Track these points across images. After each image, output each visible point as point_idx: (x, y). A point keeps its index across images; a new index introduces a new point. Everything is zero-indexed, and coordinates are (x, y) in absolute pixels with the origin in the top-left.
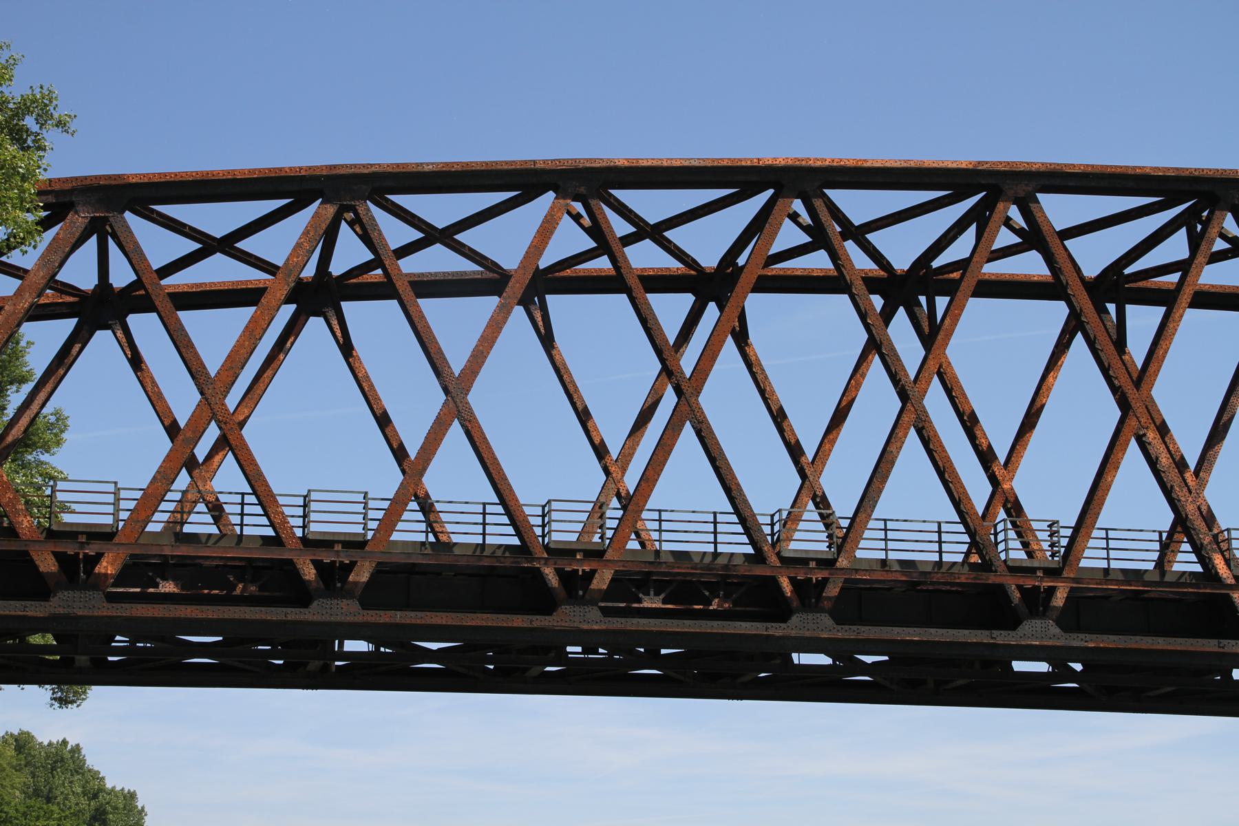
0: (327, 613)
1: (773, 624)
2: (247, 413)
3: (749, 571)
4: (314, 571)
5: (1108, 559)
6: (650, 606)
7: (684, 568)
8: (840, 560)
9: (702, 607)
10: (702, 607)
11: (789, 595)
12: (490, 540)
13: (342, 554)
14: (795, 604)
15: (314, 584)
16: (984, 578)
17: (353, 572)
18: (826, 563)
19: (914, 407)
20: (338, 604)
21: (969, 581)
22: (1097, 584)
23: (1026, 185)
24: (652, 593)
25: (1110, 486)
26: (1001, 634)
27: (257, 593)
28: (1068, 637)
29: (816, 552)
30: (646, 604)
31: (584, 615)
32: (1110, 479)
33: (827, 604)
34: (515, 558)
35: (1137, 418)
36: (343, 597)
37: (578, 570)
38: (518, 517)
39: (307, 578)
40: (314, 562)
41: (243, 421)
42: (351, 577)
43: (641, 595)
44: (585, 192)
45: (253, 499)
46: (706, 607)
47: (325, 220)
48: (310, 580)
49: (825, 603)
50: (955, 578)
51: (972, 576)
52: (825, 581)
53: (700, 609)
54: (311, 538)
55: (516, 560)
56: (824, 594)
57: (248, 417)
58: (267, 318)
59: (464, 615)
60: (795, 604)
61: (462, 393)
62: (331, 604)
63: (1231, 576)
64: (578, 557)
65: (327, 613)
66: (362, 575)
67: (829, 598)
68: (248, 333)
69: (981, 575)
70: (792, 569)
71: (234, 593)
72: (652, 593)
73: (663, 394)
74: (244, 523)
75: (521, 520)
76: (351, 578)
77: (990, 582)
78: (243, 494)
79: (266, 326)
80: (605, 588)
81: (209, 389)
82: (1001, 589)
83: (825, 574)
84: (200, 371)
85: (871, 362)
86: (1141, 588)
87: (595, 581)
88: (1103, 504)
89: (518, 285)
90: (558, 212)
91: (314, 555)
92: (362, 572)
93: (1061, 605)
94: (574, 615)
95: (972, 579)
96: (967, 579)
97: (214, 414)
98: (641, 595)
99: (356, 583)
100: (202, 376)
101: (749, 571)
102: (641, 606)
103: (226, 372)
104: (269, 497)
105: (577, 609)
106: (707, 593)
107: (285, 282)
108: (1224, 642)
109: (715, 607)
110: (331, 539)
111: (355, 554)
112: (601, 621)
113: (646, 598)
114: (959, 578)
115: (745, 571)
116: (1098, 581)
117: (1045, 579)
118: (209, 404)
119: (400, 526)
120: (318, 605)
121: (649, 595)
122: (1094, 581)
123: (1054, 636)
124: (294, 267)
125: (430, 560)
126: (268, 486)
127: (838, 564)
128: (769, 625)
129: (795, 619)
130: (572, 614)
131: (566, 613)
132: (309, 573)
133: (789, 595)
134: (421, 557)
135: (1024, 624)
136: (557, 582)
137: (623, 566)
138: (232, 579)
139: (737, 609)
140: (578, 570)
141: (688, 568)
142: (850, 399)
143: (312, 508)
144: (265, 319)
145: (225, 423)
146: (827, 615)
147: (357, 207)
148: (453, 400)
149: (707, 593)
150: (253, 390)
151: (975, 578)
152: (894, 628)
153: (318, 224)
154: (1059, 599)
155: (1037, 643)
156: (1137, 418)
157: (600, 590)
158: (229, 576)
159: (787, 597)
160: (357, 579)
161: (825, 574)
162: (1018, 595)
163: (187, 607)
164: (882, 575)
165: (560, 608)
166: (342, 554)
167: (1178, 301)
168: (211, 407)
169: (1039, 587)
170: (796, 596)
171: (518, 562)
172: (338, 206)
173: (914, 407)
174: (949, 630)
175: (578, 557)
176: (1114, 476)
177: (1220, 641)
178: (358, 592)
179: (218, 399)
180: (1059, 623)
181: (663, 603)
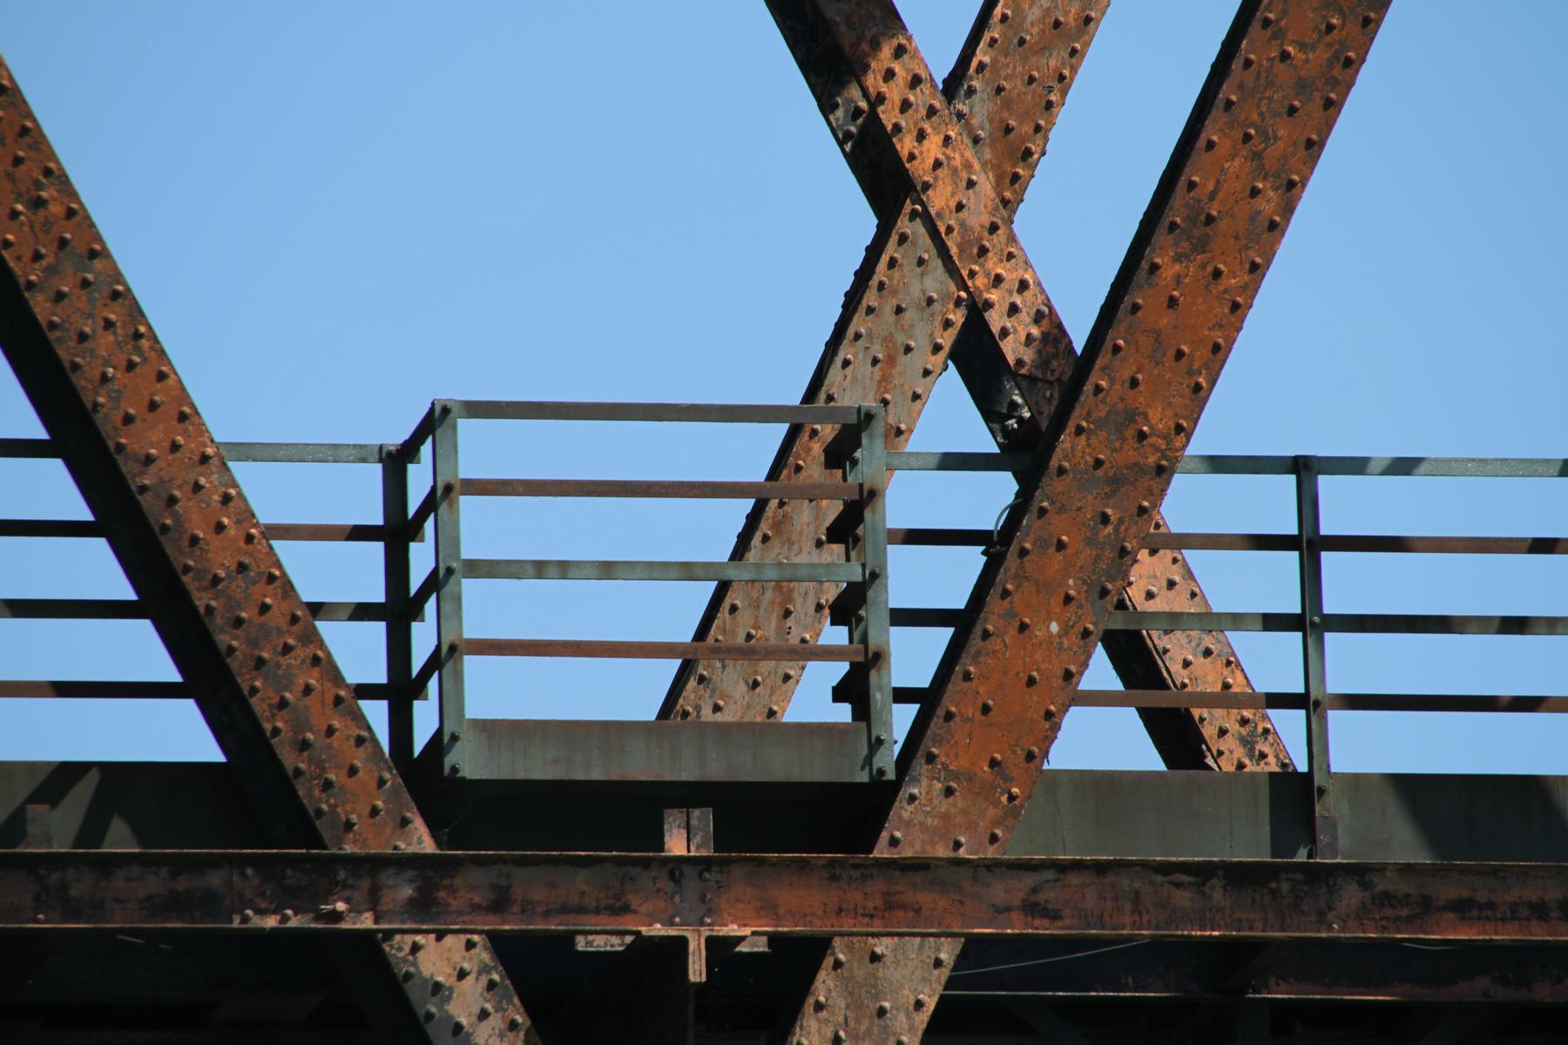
37: (683, 941)
55: (182, 884)
64: (676, 845)
75: (222, 564)
137: (1032, 908)
141: (1540, 911)
171: (210, 903)
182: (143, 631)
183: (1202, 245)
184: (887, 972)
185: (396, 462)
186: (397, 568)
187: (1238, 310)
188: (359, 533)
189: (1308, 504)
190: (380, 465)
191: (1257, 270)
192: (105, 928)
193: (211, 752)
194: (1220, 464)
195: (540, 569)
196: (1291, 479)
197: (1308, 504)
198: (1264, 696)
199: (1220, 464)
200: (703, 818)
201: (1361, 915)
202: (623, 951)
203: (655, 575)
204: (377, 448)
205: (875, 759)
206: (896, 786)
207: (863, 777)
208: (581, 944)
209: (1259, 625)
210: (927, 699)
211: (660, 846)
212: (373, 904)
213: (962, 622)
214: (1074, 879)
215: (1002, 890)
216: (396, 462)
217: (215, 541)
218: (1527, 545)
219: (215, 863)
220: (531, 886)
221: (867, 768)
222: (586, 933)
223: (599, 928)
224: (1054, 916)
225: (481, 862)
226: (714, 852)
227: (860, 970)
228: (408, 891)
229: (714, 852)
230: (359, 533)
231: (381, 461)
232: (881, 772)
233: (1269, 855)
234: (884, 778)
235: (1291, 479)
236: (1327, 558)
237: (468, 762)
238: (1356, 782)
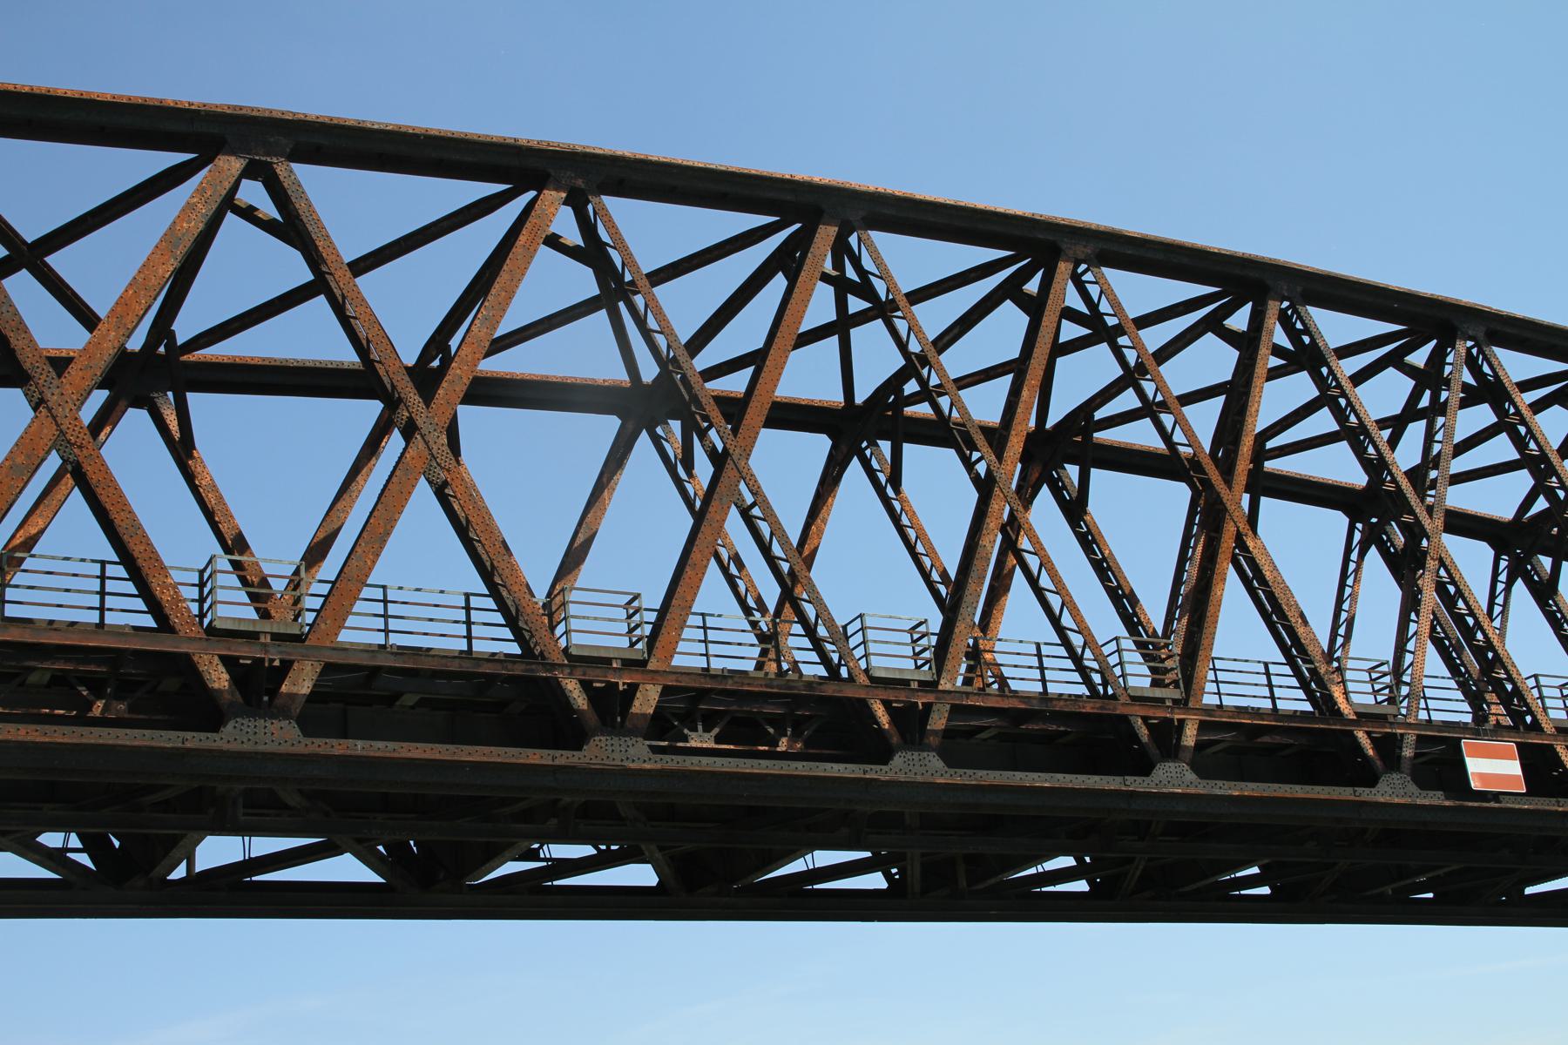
0: (249, 740)
1: (872, 767)
2: (41, 525)
3: (840, 691)
4: (226, 676)
5: (1219, 693)
6: (699, 745)
7: (757, 686)
8: (942, 682)
9: (766, 748)
10: (766, 748)
11: (887, 726)
12: (478, 646)
13: (272, 650)
14: (895, 740)
15: (227, 696)
16: (1111, 707)
17: (288, 679)
18: (929, 686)
19: (1002, 492)
20: (266, 727)
21: (1095, 711)
22: (1229, 717)
23: (1085, 247)
24: (700, 728)
25: (1221, 600)
26: (1135, 781)
27: (127, 716)
28: (1205, 784)
29: (901, 670)
30: (693, 744)
31: (626, 751)
32: (1219, 593)
33: (933, 740)
34: (528, 664)
35: (1235, 523)
36: (273, 716)
37: (618, 683)
38: (524, 607)
39: (216, 686)
40: (226, 660)
41: (35, 535)
42: (284, 686)
43: (686, 731)
44: (583, 186)
45: (120, 571)
46: (772, 749)
47: (228, 177)
48: (220, 689)
49: (932, 738)
50: (1080, 708)
51: (1098, 705)
52: (928, 707)
53: (765, 751)
54: (218, 627)
55: (528, 667)
56: (928, 727)
57: (42, 532)
58: (143, 301)
59: (457, 748)
60: (895, 740)
61: (435, 430)
62: (255, 726)
63: (1351, 712)
64: (615, 665)
65: (249, 740)
66: (301, 683)
67: (935, 732)
68: (115, 320)
69: (1108, 704)
70: (891, 691)
71: (90, 715)
72: (700, 728)
73: (597, 530)
74: (106, 606)
75: (529, 611)
76: (284, 689)
77: (1118, 712)
78: (103, 563)
79: (142, 312)
80: (652, 712)
81: (53, 394)
82: (1124, 719)
83: (930, 698)
84: (38, 367)
85: (832, 505)
86: (1273, 723)
87: (636, 703)
88: (1217, 622)
89: (504, 293)
90: (550, 207)
91: (229, 649)
92: (301, 681)
93: (1193, 744)
94: (613, 751)
95: (1098, 709)
96: (1092, 708)
97: (61, 431)
98: (686, 731)
99: (292, 696)
100: (41, 374)
101: (840, 691)
102: (688, 745)
103: (80, 373)
104: (153, 561)
105: (615, 740)
106: (771, 730)
107: (170, 254)
108: (1360, 790)
109: (784, 749)
110: (251, 629)
111: (290, 650)
112: (650, 759)
113: (693, 735)
114: (1084, 708)
115: (834, 691)
116: (1231, 714)
117: (1176, 711)
118: (54, 418)
119: (352, 620)
120: (235, 727)
121: (697, 731)
122: (1226, 714)
123: (1191, 783)
124: (184, 235)
125: (404, 662)
126: (149, 544)
127: (940, 688)
128: (868, 767)
129: (898, 760)
130: (610, 749)
131: (601, 748)
132: (219, 678)
133: (887, 726)
134: (392, 657)
135: (1157, 768)
136: (585, 702)
137: (677, 681)
138: (85, 693)
139: (811, 751)
140: (618, 683)
141: (761, 686)
142: (812, 547)
143: (219, 583)
144: (140, 303)
145: (80, 447)
146: (934, 754)
147: (275, 166)
148: (423, 439)
149: (771, 730)
150: (52, 494)
151: (1101, 708)
152: (1016, 773)
153: (218, 181)
154: (1190, 737)
155: (1180, 791)
156: (1235, 523)
157: (644, 715)
158: (80, 688)
159: (884, 729)
160: (294, 690)
161: (930, 698)
162: (1146, 732)
163: (19, 726)
164: (998, 702)
165: (592, 741)
166: (272, 650)
167: (1252, 394)
168: (56, 421)
169: (1173, 719)
170: (895, 729)
171: (532, 671)
172: (247, 160)
173: (1002, 492)
174: (1078, 776)
175: (615, 665)
176: (1223, 590)
177: (1356, 789)
178: (296, 709)
179: (67, 410)
180: (1196, 767)
181: (716, 743)
183: (694, 569)
184: (649, 693)
185: (202, 572)
186: (201, 592)
187: (701, 580)
191: (704, 574)
194: (320, 581)
195: (584, 618)
199: (320, 581)
200: (619, 661)
201: (732, 685)
202: (604, 687)
206: (648, 660)
208: (594, 685)
210: (311, 626)
211: (611, 665)
212: (562, 673)
213: (318, 611)
214: (684, 676)
215: (674, 677)
216: (202, 572)
217: (527, 608)
220: (589, 671)
222: (644, 684)
224: (681, 682)
225: (581, 666)
227: (644, 692)
228: (569, 671)
237: (574, 651)
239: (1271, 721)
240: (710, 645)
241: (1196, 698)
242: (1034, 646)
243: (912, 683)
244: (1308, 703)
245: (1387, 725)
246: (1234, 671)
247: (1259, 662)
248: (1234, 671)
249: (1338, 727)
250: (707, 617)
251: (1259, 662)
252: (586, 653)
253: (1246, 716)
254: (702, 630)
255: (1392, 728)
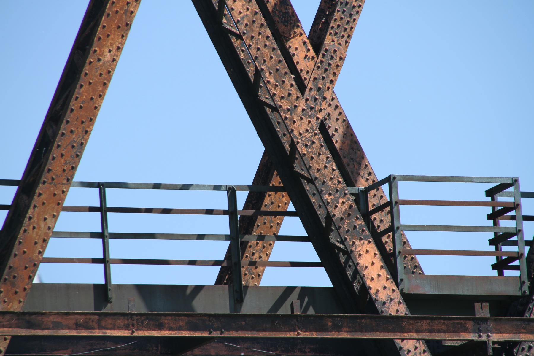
22: (78, 326)
32: (108, 57)
63: (397, 296)
176: (119, 49)
182: (309, 246)
188: (92, 209)
189: (103, 197)
190: (227, 191)
192: (325, 338)
193: (328, 283)
196: (97, 190)
197: (103, 197)
198: (91, 259)
203: (417, 229)
204: (226, 186)
205: (523, 288)
207: (519, 294)
209: (89, 236)
218: (205, 212)
219: (364, 317)
221: (520, 291)
223: (450, 339)
226: (490, 316)
229: (490, 316)
230: (92, 209)
231: (227, 190)
232: (525, 292)
233: (93, 309)
234: (526, 294)
235: (97, 190)
236: (109, 214)
238: (119, 286)
239: (179, 329)
240: (112, 242)
241: (13, 285)
242: (223, 195)
243: (477, 305)
244: (322, 270)
245: (470, 325)
246: (149, 211)
247: (217, 188)
248: (149, 211)
249: (345, 335)
250: (108, 190)
251: (217, 188)
252: (446, 291)
253: (120, 322)
254: (98, 214)
255: (479, 331)
